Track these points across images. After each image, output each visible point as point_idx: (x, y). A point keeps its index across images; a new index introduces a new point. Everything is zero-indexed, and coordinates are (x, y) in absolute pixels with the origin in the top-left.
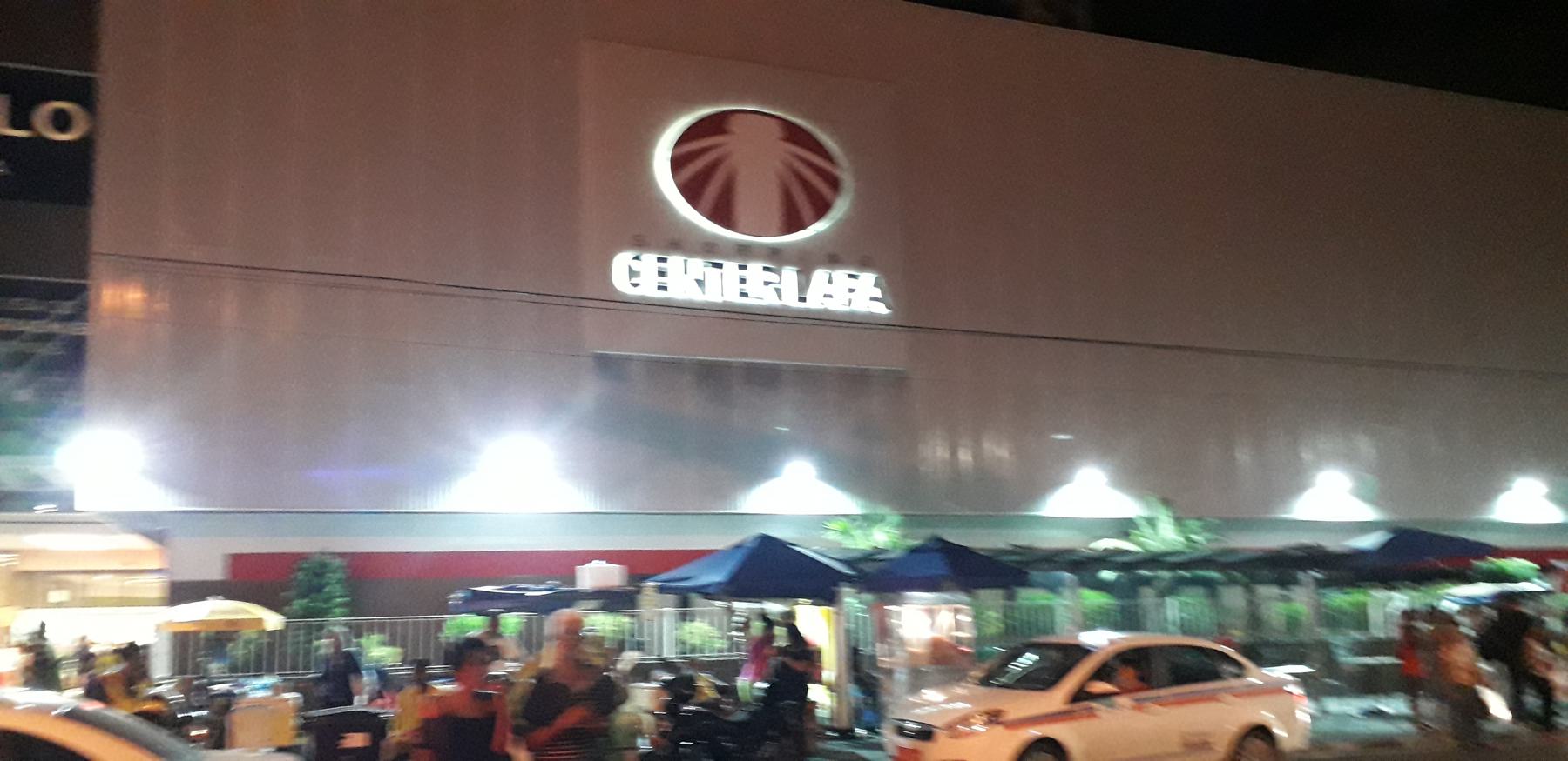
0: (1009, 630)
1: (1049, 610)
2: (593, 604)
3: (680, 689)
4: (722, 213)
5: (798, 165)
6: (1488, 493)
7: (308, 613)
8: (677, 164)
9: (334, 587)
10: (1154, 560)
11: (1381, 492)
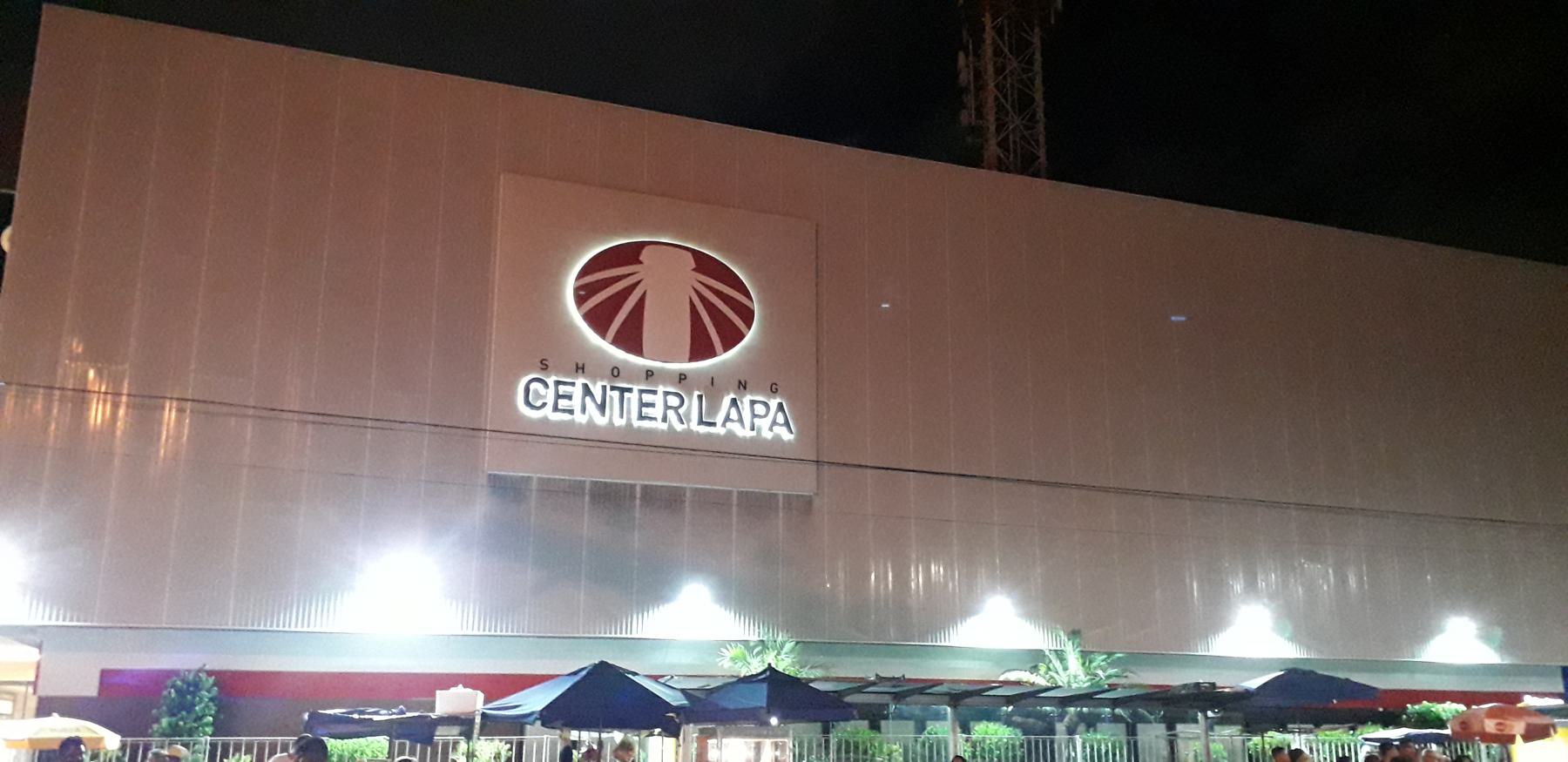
4: (630, 339)
6: (1422, 631)
9: (204, 703)
11: (1299, 622)
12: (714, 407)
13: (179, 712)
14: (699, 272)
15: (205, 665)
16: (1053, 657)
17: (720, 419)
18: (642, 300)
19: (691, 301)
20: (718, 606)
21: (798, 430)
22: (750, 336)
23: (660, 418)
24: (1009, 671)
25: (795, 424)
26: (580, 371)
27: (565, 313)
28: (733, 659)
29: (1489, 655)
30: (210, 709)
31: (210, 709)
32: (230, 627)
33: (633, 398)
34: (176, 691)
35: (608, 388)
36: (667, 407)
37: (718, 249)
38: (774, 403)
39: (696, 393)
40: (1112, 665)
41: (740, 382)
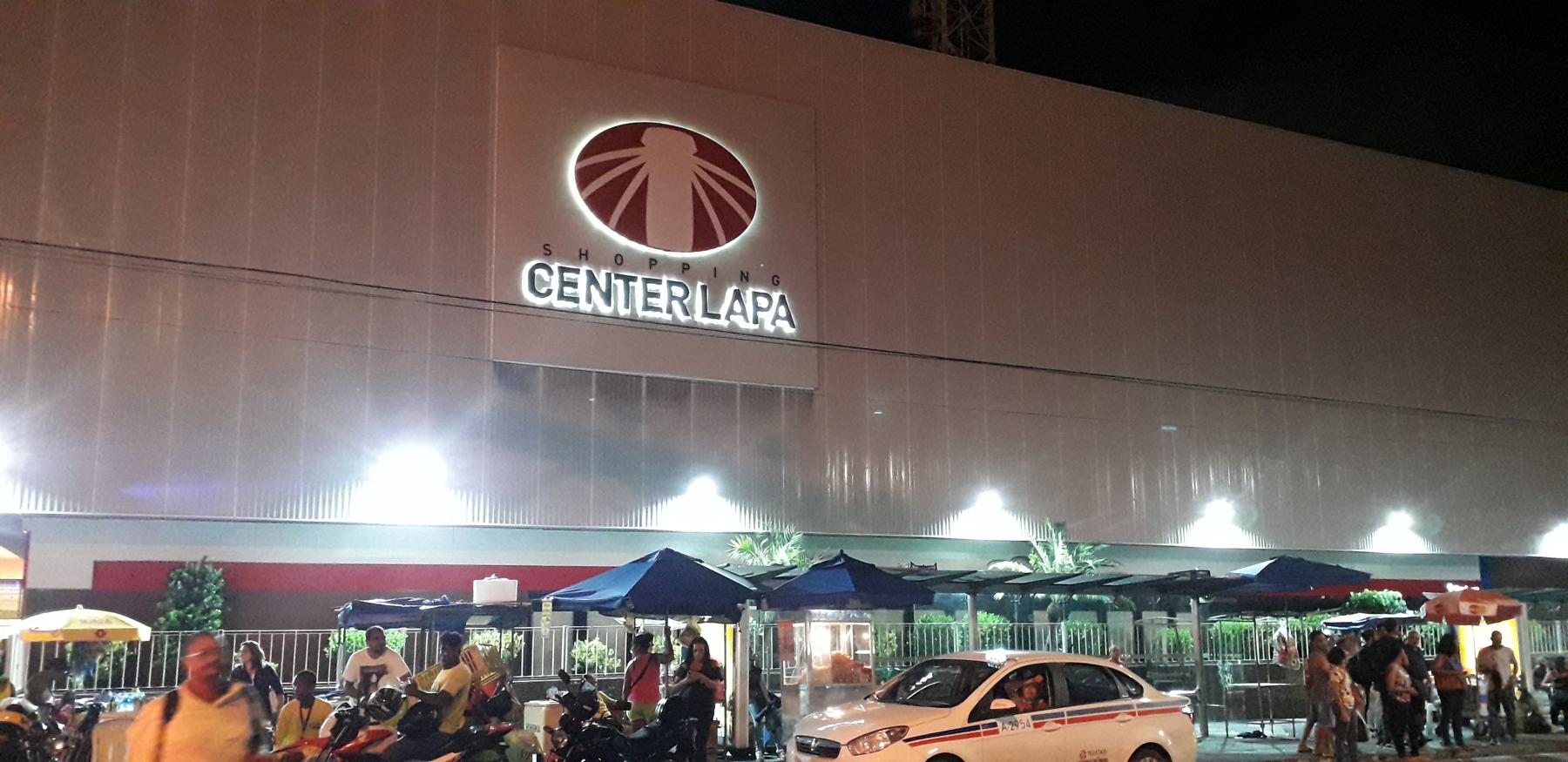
0: (906, 651)
1: (947, 632)
2: (486, 620)
3: (577, 704)
4: (633, 225)
5: (705, 177)
6: (1366, 525)
7: (184, 623)
8: (584, 178)
9: (213, 599)
10: (1050, 583)
11: (1262, 517)
12: (718, 299)
13: (187, 605)
14: (700, 157)
15: (205, 557)
16: (1039, 549)
17: (723, 311)
18: (645, 182)
19: (693, 187)
20: (725, 500)
21: (798, 323)
22: (753, 226)
23: (665, 310)
24: (995, 561)
25: (796, 317)
26: (583, 257)
27: (568, 199)
28: (741, 550)
29: (1420, 546)
30: (218, 602)
31: (218, 602)
32: (235, 517)
33: (638, 286)
34: (183, 583)
35: (613, 276)
36: (672, 297)
37: (718, 135)
38: (776, 296)
39: (700, 284)
40: (1097, 555)
41: (742, 273)
